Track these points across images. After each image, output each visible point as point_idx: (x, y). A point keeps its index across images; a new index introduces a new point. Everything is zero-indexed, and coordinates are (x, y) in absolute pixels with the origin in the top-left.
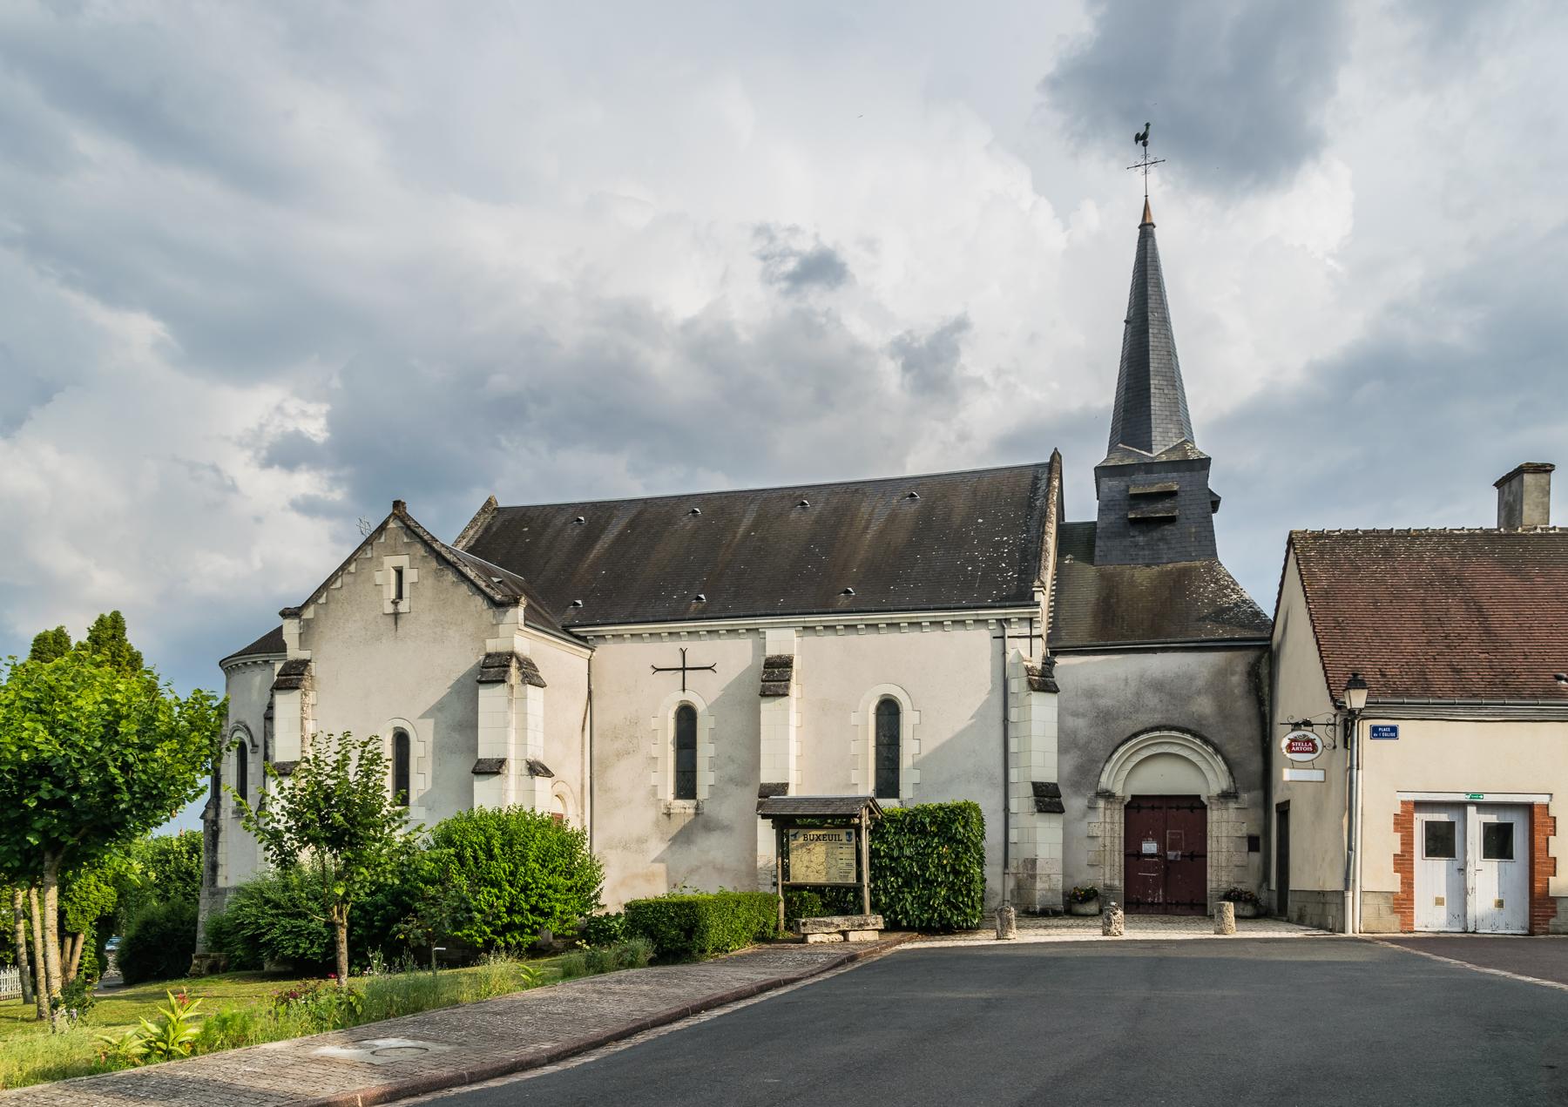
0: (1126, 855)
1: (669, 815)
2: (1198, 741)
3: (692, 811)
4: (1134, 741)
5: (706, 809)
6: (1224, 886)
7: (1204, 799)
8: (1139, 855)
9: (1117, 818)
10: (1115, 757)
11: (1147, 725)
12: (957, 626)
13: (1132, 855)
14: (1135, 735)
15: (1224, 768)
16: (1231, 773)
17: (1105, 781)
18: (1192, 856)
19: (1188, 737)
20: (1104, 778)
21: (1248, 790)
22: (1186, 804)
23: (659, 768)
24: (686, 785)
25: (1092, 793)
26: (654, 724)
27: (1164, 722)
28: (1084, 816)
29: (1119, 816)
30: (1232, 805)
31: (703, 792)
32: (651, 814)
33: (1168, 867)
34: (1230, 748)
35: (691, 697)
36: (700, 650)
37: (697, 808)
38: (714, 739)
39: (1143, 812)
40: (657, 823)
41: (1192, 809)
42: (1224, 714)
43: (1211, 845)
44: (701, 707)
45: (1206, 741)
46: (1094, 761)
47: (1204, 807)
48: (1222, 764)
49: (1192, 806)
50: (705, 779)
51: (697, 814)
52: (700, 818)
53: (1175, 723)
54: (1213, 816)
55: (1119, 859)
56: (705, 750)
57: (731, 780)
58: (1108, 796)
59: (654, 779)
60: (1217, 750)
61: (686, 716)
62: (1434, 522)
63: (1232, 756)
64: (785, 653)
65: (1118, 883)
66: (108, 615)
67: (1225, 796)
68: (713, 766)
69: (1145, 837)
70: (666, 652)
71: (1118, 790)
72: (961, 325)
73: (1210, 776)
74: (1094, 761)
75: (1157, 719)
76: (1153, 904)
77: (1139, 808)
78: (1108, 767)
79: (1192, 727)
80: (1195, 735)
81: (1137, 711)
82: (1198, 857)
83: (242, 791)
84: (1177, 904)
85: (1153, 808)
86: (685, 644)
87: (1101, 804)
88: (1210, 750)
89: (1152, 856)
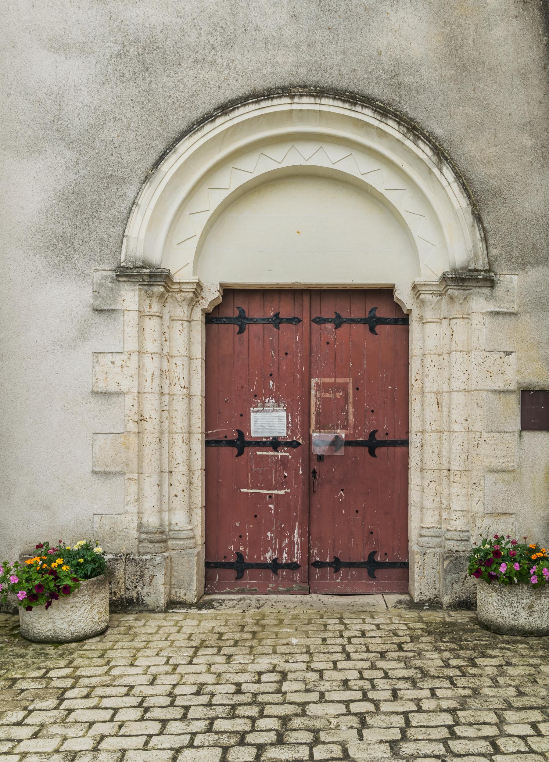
0: (209, 443)
2: (391, 128)
4: (222, 124)
6: (458, 523)
7: (404, 295)
8: (242, 443)
9: (179, 342)
10: (170, 166)
11: (259, 83)
13: (226, 443)
14: (226, 108)
15: (460, 201)
16: (478, 218)
17: (142, 240)
18: (372, 444)
19: (366, 115)
20: (137, 227)
21: (521, 264)
22: (358, 310)
25: (103, 271)
27: (303, 75)
28: (84, 334)
29: (186, 340)
30: (479, 303)
33: (314, 472)
34: (474, 150)
39: (251, 328)
41: (372, 323)
42: (461, 60)
43: (421, 415)
45: (414, 129)
46: (110, 180)
47: (402, 320)
48: (454, 191)
49: (378, 311)
53: (331, 80)
54: (425, 338)
55: (188, 454)
58: (151, 278)
60: (442, 154)
63: (479, 172)
65: (186, 519)
66: (91, 301)
67: (465, 280)
69: (258, 396)
71: (182, 269)
72: (378, 430)
73: (420, 228)
74: (110, 180)
75: (284, 66)
76: (275, 566)
77: (242, 322)
78: (150, 196)
79: (376, 91)
80: (384, 111)
81: (229, 44)
82: (383, 446)
84: (337, 565)
85: (277, 321)
87: (130, 297)
88: (424, 152)
89: (275, 444)
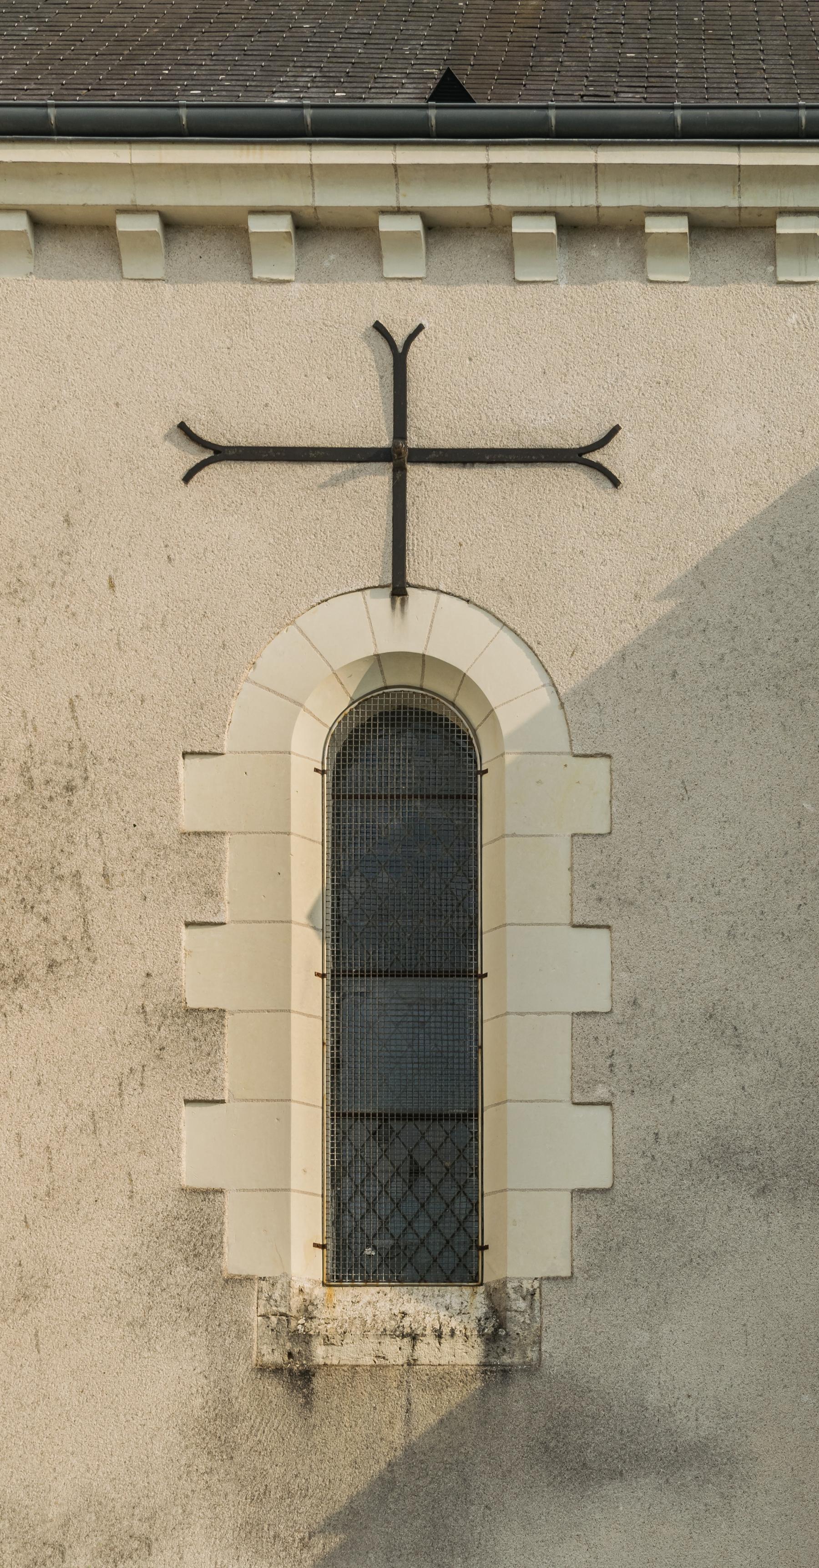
1: (299, 1376)
3: (466, 1354)
5: (559, 1340)
12: (725, 256)
23: (231, 1077)
24: (409, 1179)
26: (198, 795)
31: (529, 1232)
32: (172, 1376)
35: (442, 630)
36: (505, 345)
37: (495, 1331)
38: (605, 895)
40: (216, 1430)
44: (512, 696)
50: (544, 1157)
51: (495, 1373)
52: (517, 1398)
56: (542, 972)
57: (725, 1157)
59: (200, 1149)
61: (408, 766)
62: (781, 163)
64: (418, 324)
68: (604, 1065)
70: (289, 344)
83: (383, 34)
86: (408, 292)
